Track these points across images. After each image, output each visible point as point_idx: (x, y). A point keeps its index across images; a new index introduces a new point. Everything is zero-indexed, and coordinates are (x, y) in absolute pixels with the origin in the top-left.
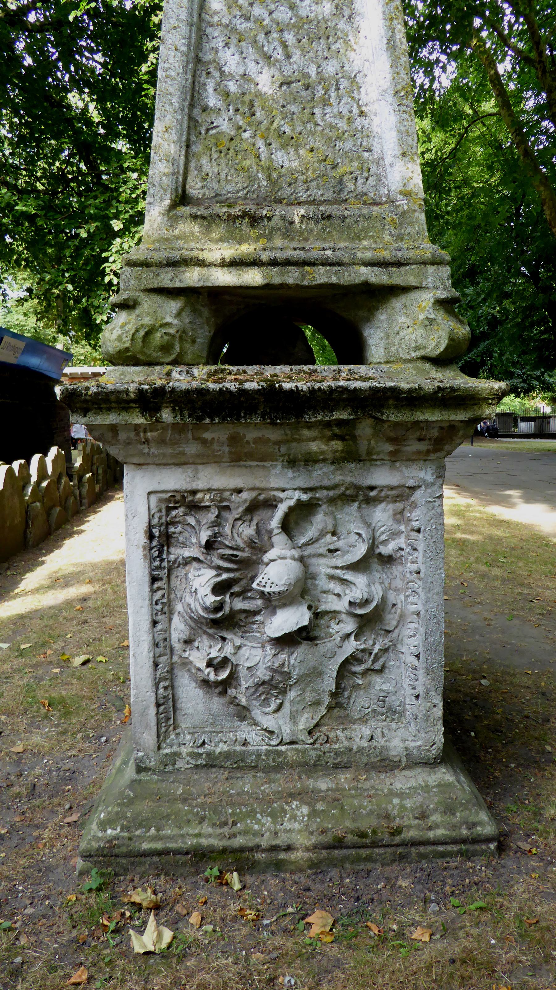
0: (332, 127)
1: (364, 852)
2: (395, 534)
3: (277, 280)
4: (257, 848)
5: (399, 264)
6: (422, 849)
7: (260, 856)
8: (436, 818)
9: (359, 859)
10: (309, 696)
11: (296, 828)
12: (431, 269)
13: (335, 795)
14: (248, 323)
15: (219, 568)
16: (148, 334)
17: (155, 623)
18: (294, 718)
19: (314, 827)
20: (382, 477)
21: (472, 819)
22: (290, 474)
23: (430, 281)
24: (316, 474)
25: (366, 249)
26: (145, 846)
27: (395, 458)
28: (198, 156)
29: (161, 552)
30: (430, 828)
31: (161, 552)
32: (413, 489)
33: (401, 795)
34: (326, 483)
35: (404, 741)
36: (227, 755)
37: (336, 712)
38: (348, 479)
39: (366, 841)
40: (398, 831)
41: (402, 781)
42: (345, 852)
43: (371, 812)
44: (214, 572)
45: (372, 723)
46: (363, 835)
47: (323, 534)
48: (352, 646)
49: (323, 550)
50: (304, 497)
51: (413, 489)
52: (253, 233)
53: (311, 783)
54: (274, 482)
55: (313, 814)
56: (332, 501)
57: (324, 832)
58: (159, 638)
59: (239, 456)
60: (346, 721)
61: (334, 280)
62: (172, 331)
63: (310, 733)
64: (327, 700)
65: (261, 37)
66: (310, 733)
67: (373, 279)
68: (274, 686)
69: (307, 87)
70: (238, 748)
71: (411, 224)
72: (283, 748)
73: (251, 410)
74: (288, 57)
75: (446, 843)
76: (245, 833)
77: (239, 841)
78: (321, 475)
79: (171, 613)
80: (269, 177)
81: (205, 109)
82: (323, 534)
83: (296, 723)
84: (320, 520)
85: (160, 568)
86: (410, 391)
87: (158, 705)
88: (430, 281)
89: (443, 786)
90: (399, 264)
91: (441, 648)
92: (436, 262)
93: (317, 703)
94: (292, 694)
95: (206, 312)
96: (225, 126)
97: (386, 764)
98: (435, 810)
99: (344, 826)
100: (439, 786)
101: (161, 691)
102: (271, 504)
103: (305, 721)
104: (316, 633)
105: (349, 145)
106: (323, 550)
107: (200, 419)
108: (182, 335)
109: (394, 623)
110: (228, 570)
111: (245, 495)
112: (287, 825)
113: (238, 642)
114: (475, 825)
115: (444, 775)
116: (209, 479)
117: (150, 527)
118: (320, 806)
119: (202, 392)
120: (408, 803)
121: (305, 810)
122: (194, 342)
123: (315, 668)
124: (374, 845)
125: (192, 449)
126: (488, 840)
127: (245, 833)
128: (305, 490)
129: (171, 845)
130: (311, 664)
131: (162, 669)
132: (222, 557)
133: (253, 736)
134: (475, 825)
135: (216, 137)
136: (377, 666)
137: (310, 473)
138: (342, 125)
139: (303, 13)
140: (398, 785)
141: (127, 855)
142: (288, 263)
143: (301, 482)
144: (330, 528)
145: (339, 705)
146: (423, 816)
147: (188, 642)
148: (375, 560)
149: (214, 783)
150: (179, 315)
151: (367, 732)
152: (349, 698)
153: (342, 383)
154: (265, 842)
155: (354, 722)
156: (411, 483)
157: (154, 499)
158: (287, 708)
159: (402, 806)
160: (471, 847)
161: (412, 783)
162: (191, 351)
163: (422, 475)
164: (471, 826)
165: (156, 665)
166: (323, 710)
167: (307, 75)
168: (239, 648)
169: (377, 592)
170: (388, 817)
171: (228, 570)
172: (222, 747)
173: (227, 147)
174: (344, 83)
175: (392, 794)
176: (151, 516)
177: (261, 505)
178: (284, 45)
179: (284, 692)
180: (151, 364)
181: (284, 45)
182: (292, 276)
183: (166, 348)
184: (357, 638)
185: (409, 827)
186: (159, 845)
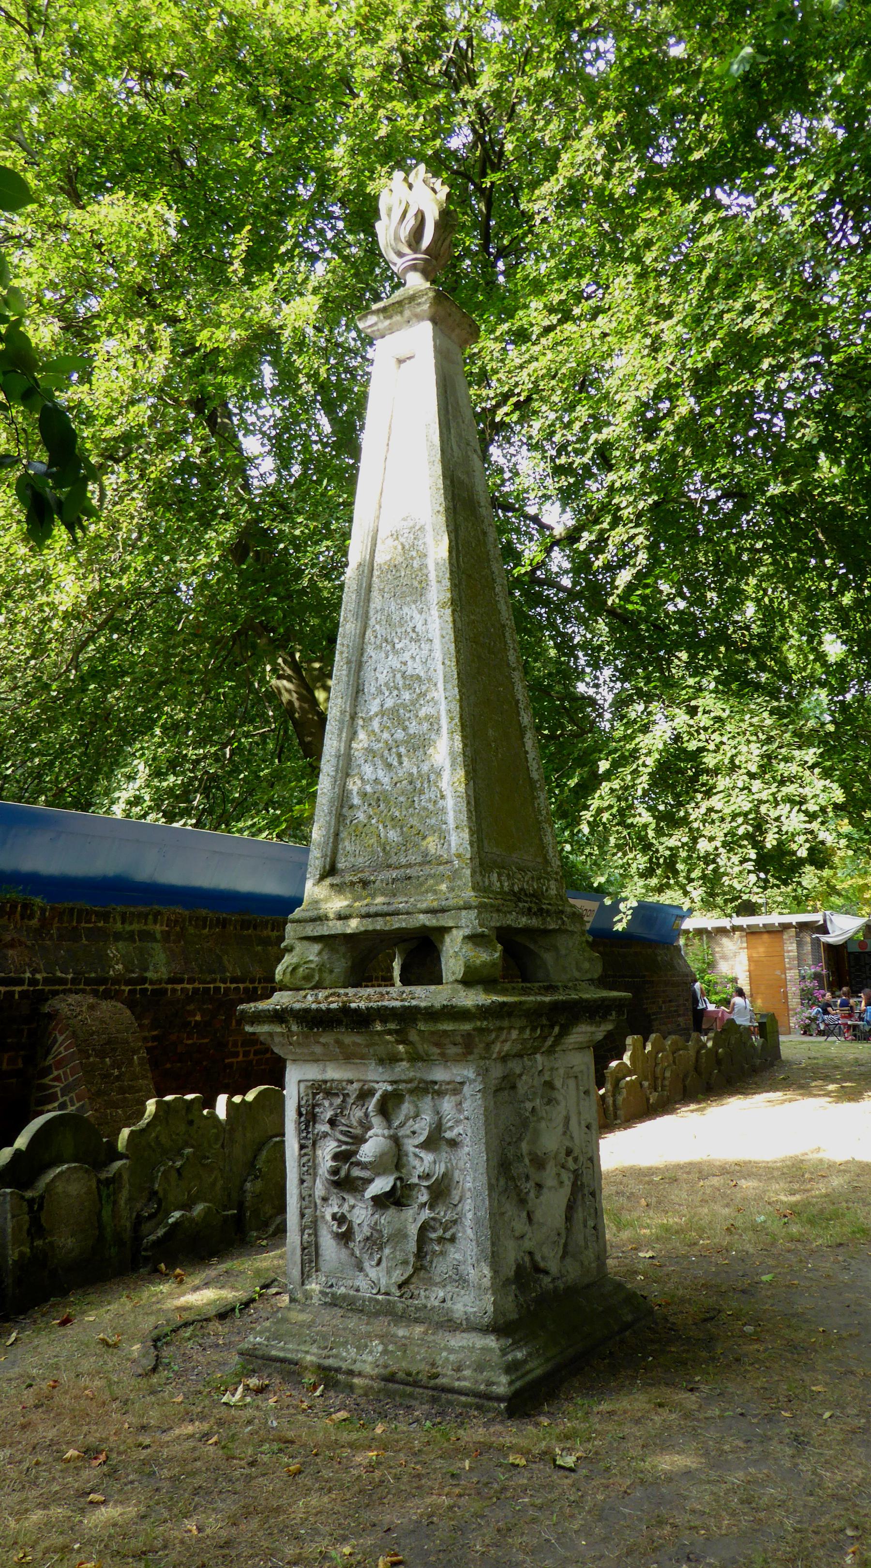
0: (425, 809)
1: (409, 1389)
2: (458, 1122)
3: (370, 928)
4: (338, 1370)
5: (443, 910)
6: (449, 1396)
7: (341, 1377)
8: (467, 1373)
9: (404, 1395)
10: (399, 1256)
11: (367, 1360)
12: (464, 913)
13: (407, 1342)
14: (363, 956)
15: (339, 1141)
16: (294, 969)
17: (302, 1181)
18: (389, 1272)
19: (381, 1362)
20: (440, 1074)
21: (494, 1379)
22: (380, 1070)
23: (463, 922)
24: (398, 1069)
25: (430, 901)
26: (274, 1353)
27: (445, 1059)
28: (343, 840)
29: (307, 1127)
30: (458, 1379)
31: (307, 1127)
32: (462, 1084)
33: (451, 1351)
34: (403, 1077)
35: (465, 1305)
36: (344, 1297)
37: (422, 1273)
38: (418, 1075)
39: (411, 1381)
40: (436, 1376)
41: (458, 1341)
42: (396, 1386)
43: (424, 1359)
44: (335, 1144)
45: (449, 1288)
46: (409, 1374)
47: (407, 1119)
48: (426, 1214)
49: (408, 1132)
50: (390, 1088)
51: (462, 1084)
52: (364, 893)
53: (393, 1329)
54: (371, 1076)
55: (385, 1352)
56: (411, 1092)
57: (386, 1367)
58: (305, 1193)
59: (348, 1056)
60: (430, 1283)
61: (404, 925)
62: (313, 966)
63: (400, 1287)
64: (412, 1259)
65: (386, 753)
66: (400, 1287)
67: (428, 923)
68: (375, 1242)
69: (411, 783)
70: (352, 1292)
71: (460, 878)
72: (380, 1297)
73: (339, 1023)
74: (401, 763)
75: (467, 1395)
76: (335, 1356)
77: (330, 1362)
78: (402, 1069)
79: (315, 1175)
80: (384, 850)
81: (351, 807)
82: (407, 1119)
83: (390, 1277)
84: (406, 1108)
85: (306, 1138)
86: (426, 1008)
87: (303, 1249)
88: (463, 922)
89: (485, 1349)
90: (443, 910)
91: (487, 1223)
92: (467, 907)
93: (405, 1263)
94: (387, 1251)
95: (343, 949)
96: (361, 816)
97: (451, 1325)
98: (469, 1367)
99: (399, 1365)
100: (482, 1349)
101: (306, 1236)
102: (371, 1093)
103: (398, 1276)
104: (404, 1201)
105: (433, 821)
106: (408, 1132)
107: (311, 1029)
108: (321, 968)
109: (457, 1198)
110: (346, 1143)
111: (356, 1085)
112: (364, 1357)
113: (352, 1201)
114: (493, 1384)
115: (491, 1342)
116: (334, 1073)
117: (299, 1106)
118: (391, 1348)
119: (307, 1011)
120: (452, 1357)
121: (380, 1348)
122: (331, 971)
123: (400, 1230)
124: (416, 1384)
125: (318, 1050)
126: (499, 1399)
127: (335, 1356)
128: (392, 1083)
129: (289, 1356)
130: (397, 1226)
131: (307, 1220)
132: (342, 1132)
133: (361, 1282)
134: (493, 1384)
135: (356, 826)
136: (448, 1235)
137: (393, 1069)
138: (431, 806)
139: (411, 731)
140: (452, 1343)
141: (263, 1357)
142: (377, 915)
143: (386, 1077)
144: (412, 1114)
145: (423, 1268)
146: (458, 1369)
147: (325, 1199)
148: (435, 1140)
149: (332, 1318)
150: (320, 953)
151: (441, 1294)
152: (431, 1262)
153: (386, 1003)
154: (344, 1366)
155: (436, 1284)
156: (459, 1079)
157: (302, 1085)
158: (384, 1264)
159: (447, 1359)
160: (486, 1403)
161: (464, 1343)
162: (328, 978)
163: (465, 1073)
164: (490, 1384)
165: (302, 1215)
166: (410, 1270)
167: (411, 774)
168: (353, 1207)
169: (440, 1169)
170: (433, 1365)
171: (346, 1143)
172: (343, 1290)
173: (359, 833)
174: (433, 777)
175: (446, 1348)
176: (300, 1099)
177: (365, 1095)
178: (400, 756)
179: (381, 1249)
180: (298, 989)
181: (400, 756)
182: (379, 924)
183: (307, 978)
184: (432, 1208)
185: (445, 1376)
186: (281, 1354)
